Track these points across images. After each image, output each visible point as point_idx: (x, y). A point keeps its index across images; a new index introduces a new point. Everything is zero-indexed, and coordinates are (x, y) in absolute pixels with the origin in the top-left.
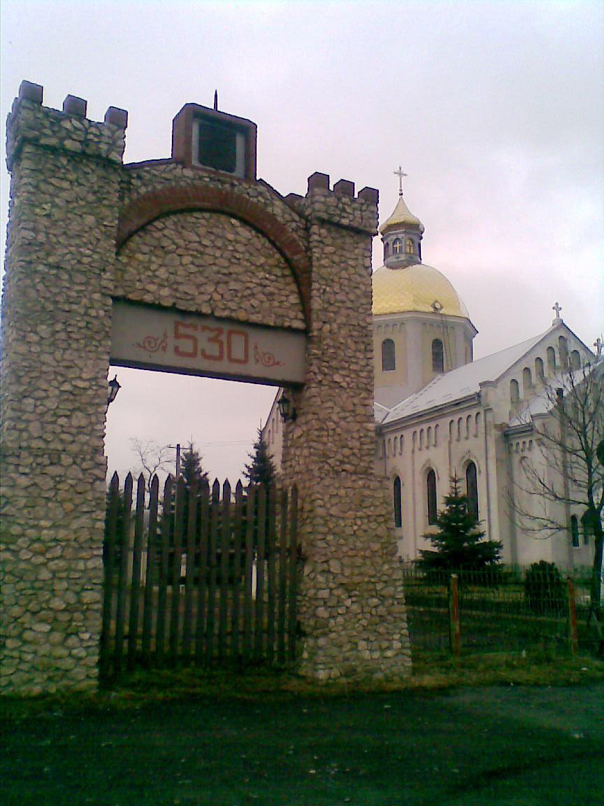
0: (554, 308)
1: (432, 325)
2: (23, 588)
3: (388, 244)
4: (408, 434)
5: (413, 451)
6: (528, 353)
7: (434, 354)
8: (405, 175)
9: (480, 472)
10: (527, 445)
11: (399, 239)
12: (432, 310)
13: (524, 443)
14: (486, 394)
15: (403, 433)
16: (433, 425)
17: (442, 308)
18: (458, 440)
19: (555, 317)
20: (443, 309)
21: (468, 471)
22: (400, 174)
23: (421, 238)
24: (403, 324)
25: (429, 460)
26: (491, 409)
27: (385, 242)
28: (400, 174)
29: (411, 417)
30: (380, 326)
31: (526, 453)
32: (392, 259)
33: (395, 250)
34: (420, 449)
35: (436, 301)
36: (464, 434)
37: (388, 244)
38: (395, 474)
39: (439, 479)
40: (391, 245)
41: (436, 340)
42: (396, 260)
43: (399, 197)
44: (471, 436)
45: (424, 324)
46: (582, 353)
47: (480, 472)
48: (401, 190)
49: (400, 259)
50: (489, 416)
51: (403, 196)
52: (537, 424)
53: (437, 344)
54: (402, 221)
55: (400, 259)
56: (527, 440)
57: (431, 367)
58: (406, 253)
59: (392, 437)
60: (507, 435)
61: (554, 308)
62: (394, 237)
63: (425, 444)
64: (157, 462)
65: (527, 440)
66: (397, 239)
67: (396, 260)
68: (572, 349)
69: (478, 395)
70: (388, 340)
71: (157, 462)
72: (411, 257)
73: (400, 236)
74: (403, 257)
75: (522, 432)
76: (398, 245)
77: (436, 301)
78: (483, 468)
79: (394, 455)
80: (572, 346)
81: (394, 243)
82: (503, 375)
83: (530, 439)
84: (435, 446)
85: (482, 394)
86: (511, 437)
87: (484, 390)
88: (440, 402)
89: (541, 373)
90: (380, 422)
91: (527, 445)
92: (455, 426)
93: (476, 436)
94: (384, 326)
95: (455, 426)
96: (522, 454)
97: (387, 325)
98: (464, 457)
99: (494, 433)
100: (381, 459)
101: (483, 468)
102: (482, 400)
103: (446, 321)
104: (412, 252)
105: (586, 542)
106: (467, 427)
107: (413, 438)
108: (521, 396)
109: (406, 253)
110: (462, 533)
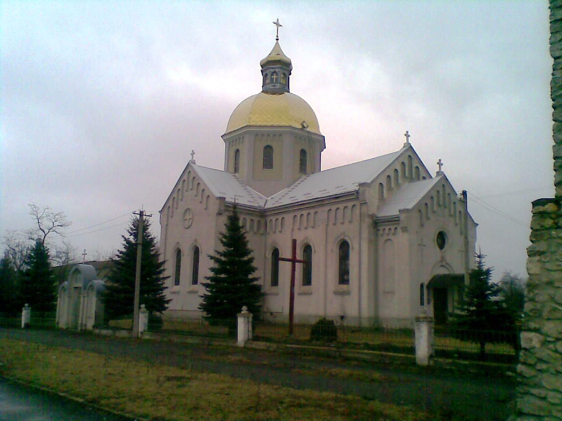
0: (438, 164)
1: (300, 138)
2: (545, 359)
3: (267, 74)
4: (288, 218)
5: (293, 230)
6: (390, 165)
7: (301, 160)
8: (281, 26)
9: (315, 251)
10: (393, 231)
11: (276, 72)
12: (300, 127)
13: (390, 229)
14: (364, 192)
15: (284, 216)
16: (312, 211)
17: (308, 127)
18: (334, 224)
19: (406, 141)
20: (308, 128)
21: (265, 153)
22: (277, 24)
23: (290, 74)
24: (280, 135)
25: (306, 238)
26: (366, 203)
27: (264, 73)
28: (277, 24)
29: (292, 205)
30: (263, 135)
31: (391, 237)
32: (270, 87)
33: (272, 79)
34: (299, 229)
35: (304, 122)
36: (340, 220)
37: (267, 74)
38: (178, 248)
39: (183, 255)
40: (269, 77)
41: (302, 150)
42: (273, 88)
43: (276, 41)
44: (346, 221)
45: (296, 137)
46: (421, 169)
47: (315, 251)
48: (277, 36)
49: (275, 87)
50: (364, 208)
51: (278, 41)
52: (403, 217)
53: (303, 152)
54: (279, 59)
55: (275, 87)
56: (393, 227)
57: (298, 169)
58: (281, 83)
59: (274, 218)
60: (377, 223)
61: (405, 135)
62: (272, 70)
63: (305, 225)
64: (51, 225)
65: (393, 227)
66: (275, 72)
67: (273, 88)
68: (416, 165)
69: (357, 192)
70: (268, 146)
71: (51, 225)
72: (283, 87)
73: (277, 70)
74: (278, 86)
75: (391, 221)
76: (275, 77)
77: (304, 122)
78: (356, 246)
79: (275, 232)
80: (415, 164)
81: (272, 74)
82: (373, 180)
83: (389, 227)
84: (313, 227)
85: (360, 191)
86: (379, 224)
87: (361, 189)
88: (317, 194)
89: (397, 180)
90: (263, 206)
91: (393, 231)
92: (333, 213)
93: (350, 222)
94: (271, 135)
95: (333, 213)
96: (390, 237)
97: (275, 135)
98: (340, 236)
99: (368, 221)
100: (262, 234)
101: (356, 246)
102: (361, 198)
103: (311, 137)
104: (284, 83)
105: (429, 303)
106: (344, 215)
107: (294, 221)
108: (385, 195)
109: (281, 83)
110: (214, 289)
